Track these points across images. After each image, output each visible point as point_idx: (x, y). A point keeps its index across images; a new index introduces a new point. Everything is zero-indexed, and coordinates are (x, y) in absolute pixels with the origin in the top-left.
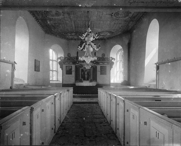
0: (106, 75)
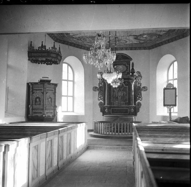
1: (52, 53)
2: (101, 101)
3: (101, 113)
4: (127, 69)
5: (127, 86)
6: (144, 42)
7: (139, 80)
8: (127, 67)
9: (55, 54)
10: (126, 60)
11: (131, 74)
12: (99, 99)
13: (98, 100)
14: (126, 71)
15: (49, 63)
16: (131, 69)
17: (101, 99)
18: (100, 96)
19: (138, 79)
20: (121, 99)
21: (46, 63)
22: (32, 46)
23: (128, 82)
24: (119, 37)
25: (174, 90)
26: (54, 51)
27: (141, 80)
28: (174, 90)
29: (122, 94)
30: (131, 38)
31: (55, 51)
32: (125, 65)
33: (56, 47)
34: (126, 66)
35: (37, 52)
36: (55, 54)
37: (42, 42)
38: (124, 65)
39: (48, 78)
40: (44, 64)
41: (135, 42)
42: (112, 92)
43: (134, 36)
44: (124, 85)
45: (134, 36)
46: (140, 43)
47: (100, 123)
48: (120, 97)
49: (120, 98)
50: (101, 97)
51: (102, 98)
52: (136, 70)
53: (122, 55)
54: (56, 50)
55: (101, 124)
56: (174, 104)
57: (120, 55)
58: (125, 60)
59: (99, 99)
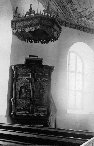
15: (45, 40)
40: (38, 42)
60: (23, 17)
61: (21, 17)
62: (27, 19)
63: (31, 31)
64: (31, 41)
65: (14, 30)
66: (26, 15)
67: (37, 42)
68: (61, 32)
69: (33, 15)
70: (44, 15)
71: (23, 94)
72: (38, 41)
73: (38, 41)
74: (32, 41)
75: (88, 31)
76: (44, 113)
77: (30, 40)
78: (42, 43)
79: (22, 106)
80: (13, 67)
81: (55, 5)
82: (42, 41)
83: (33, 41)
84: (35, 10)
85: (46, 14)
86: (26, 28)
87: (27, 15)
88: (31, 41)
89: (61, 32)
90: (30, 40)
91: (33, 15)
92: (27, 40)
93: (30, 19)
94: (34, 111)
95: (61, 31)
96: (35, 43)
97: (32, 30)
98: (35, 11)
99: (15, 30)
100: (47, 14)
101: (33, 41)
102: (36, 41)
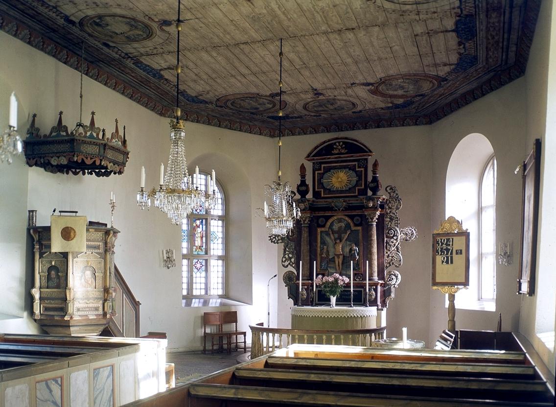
0: (468, 285)
1: (84, 142)
2: (291, 269)
3: (291, 301)
4: (319, 180)
5: (360, 228)
6: (404, 103)
7: (394, 211)
8: (359, 175)
9: (95, 144)
10: (356, 156)
11: (370, 193)
12: (286, 263)
13: (283, 266)
14: (357, 185)
15: (103, 171)
16: (370, 179)
17: (289, 264)
18: (287, 256)
19: (390, 208)
20: (343, 263)
21: (95, 172)
22: (36, 125)
23: (361, 216)
24: (324, 92)
25: (464, 238)
26: (91, 136)
27: (397, 208)
28: (464, 238)
29: (347, 250)
30: (362, 92)
31: (95, 139)
32: (352, 168)
33: (96, 126)
34: (356, 172)
35: (46, 142)
36: (95, 144)
37: (93, 113)
38: (350, 169)
39: (76, 212)
40: (92, 174)
41: (378, 103)
42: (319, 245)
43: (364, 84)
44: (352, 224)
45: (364, 84)
46: (397, 106)
47: (265, 334)
48: (339, 258)
49: (340, 262)
50: (290, 258)
51: (293, 260)
52: (384, 180)
53: (344, 143)
54: (98, 135)
55: (268, 336)
56: (463, 281)
57: (339, 142)
58: (352, 156)
59: (286, 263)
60: (45, 136)
61: (42, 136)
62: (56, 141)
63: (61, 164)
64: (76, 171)
65: (30, 159)
66: (51, 133)
67: (89, 173)
68: (127, 159)
69: (64, 134)
70: (85, 137)
71: (53, 280)
72: (89, 171)
73: (89, 171)
74: (78, 170)
75: (230, 126)
76: (96, 313)
77: (74, 170)
78: (98, 175)
79: (51, 301)
80: (32, 231)
81: (139, 85)
82: (97, 171)
83: (79, 172)
84: (67, 126)
85: (88, 134)
86: (52, 157)
87: (54, 134)
88: (76, 171)
89: (127, 159)
90: (74, 170)
91: (64, 134)
92: (65, 170)
93: (59, 142)
94: (75, 311)
95: (128, 158)
96: (84, 174)
97: (63, 163)
98: (67, 127)
99: (31, 159)
100: (91, 133)
101: (80, 171)
102: (86, 171)
